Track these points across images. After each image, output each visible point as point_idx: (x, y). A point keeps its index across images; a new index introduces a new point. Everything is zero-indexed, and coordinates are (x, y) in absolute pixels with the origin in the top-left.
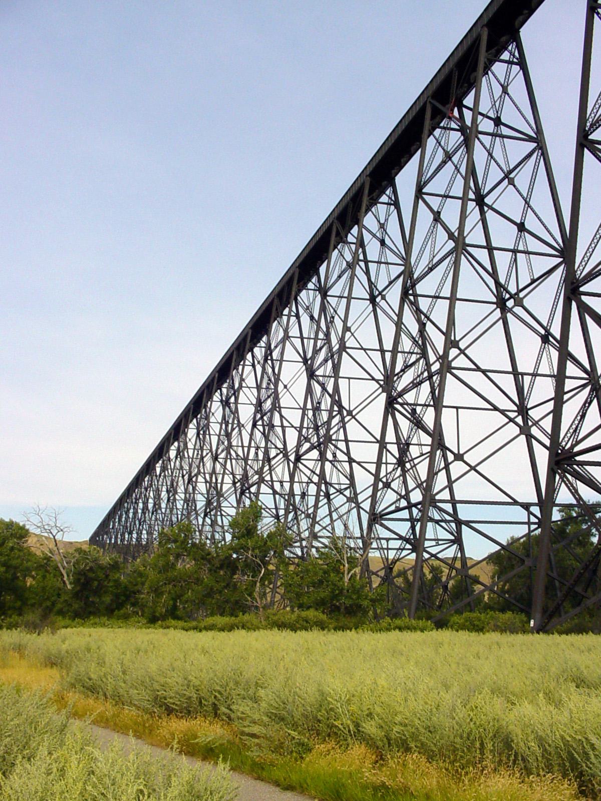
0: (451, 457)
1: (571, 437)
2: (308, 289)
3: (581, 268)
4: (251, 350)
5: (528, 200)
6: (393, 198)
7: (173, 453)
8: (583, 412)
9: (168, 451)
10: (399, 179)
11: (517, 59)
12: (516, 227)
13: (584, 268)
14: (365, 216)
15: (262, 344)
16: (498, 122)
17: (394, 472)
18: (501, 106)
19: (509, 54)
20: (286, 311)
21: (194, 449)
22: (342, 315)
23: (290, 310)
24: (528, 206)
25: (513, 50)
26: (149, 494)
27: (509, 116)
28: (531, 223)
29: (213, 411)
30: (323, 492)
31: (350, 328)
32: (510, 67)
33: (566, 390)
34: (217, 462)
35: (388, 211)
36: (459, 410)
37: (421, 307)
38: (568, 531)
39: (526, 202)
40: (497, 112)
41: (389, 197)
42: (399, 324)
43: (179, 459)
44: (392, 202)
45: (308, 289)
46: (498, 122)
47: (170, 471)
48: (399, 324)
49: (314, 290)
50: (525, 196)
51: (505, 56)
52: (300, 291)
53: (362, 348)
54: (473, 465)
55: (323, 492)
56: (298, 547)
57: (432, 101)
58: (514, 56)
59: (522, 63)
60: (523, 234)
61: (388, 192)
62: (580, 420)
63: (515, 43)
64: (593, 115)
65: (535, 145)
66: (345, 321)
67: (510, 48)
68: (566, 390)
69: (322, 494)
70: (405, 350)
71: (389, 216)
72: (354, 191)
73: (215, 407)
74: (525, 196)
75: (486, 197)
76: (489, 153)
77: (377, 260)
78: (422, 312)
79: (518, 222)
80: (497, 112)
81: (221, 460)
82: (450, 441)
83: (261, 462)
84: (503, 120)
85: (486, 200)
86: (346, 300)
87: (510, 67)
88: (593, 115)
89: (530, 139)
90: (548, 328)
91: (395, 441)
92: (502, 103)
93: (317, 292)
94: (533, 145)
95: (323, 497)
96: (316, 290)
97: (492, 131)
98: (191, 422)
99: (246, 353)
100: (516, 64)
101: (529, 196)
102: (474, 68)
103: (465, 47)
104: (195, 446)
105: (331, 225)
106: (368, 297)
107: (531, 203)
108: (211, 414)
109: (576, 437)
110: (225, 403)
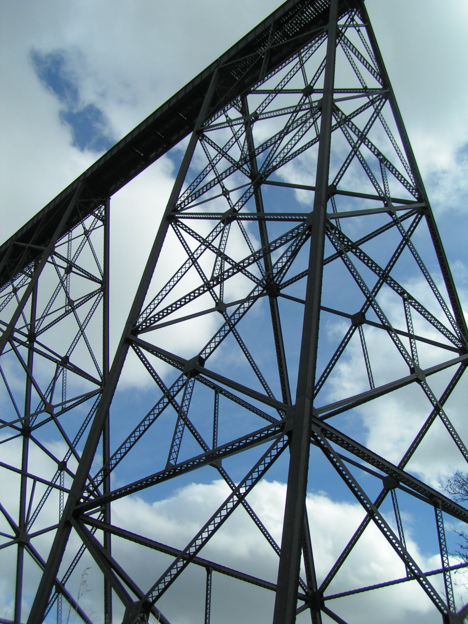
1: (276, 158)
3: (99, 298)
5: (83, 327)
8: (296, 246)
12: (57, 465)
13: (97, 298)
17: (42, 319)
33: (86, 549)
38: (461, 346)
39: (82, 332)
42: (277, 92)
48: (277, 92)
59: (105, 283)
60: (62, 473)
62: (290, 257)
64: (148, 311)
68: (86, 549)
75: (33, 430)
88: (148, 311)
90: (70, 452)
101: (85, 324)
109: (293, 118)
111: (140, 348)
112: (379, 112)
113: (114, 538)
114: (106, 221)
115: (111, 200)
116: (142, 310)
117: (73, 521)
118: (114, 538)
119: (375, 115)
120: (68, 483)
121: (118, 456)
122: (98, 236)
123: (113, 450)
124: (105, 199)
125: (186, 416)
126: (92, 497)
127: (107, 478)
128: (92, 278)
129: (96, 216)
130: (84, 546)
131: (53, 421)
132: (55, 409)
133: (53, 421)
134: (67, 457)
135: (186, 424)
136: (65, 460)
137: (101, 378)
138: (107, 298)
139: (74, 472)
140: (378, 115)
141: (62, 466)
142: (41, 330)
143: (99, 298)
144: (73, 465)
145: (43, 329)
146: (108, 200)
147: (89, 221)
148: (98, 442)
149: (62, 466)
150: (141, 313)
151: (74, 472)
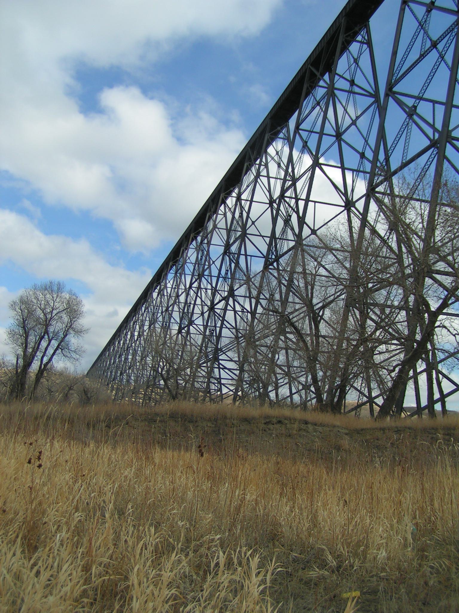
2: (233, 197)
4: (224, 202)
7: (155, 295)
9: (151, 294)
10: (375, 21)
11: (366, 40)
14: (339, 59)
15: (234, 194)
16: (352, 83)
19: (361, 37)
20: (258, 162)
21: (172, 288)
23: (261, 161)
25: (364, 34)
26: (136, 326)
27: (359, 80)
29: (189, 255)
32: (361, 45)
34: (191, 290)
35: (360, 49)
37: (210, 286)
41: (284, 134)
43: (160, 296)
45: (233, 197)
46: (352, 83)
47: (152, 307)
50: (365, 137)
51: (359, 38)
52: (226, 198)
53: (261, 236)
57: (312, 68)
58: (365, 39)
59: (369, 43)
61: (283, 131)
63: (365, 29)
65: (374, 99)
67: (362, 33)
70: (363, 174)
71: (361, 55)
72: (261, 129)
73: (192, 254)
74: (365, 137)
76: (345, 109)
77: (275, 177)
78: (296, 212)
79: (361, 152)
81: (194, 289)
84: (356, 82)
85: (343, 137)
86: (317, 135)
87: (361, 45)
89: (371, 95)
93: (286, 141)
94: (373, 99)
96: (285, 139)
97: (348, 89)
98: (191, 244)
99: (336, 58)
100: (365, 43)
101: (368, 137)
102: (333, 53)
103: (332, 32)
104: (172, 286)
105: (246, 152)
106: (334, 134)
107: (369, 142)
108: (187, 258)
110: (199, 249)
114: (369, 43)
115: (370, 23)
120: (368, 167)
121: (392, 148)
122: (365, 61)
123: (389, 146)
124: (365, 24)
125: (427, 32)
127: (388, 162)
129: (360, 42)
130: (383, 200)
134: (364, 148)
135: (428, 37)
136: (363, 152)
137: (374, 92)
138: (369, 35)
139: (371, 159)
141: (362, 155)
144: (369, 154)
146: (367, 23)
147: (354, 47)
148: (380, 145)
149: (362, 155)
151: (371, 159)
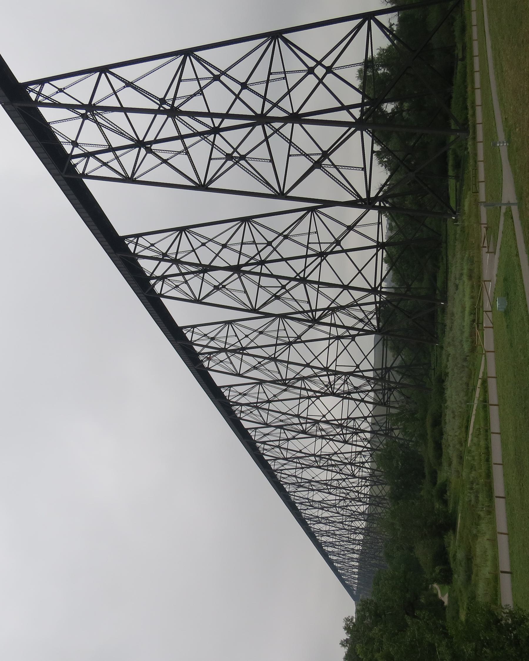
0: (358, 370)
3: (179, 119)
6: (227, 388)
18: (66, 138)
22: (294, 453)
24: (212, 240)
28: (223, 240)
30: (347, 396)
31: (300, 450)
32: (150, 273)
33: (116, 152)
36: (337, 365)
40: (69, 142)
44: (229, 389)
49: (256, 432)
54: (367, 357)
55: (347, 396)
56: (383, 288)
66: (297, 452)
68: (116, 152)
69: (348, 396)
80: (69, 142)
82: (352, 369)
83: (339, 495)
87: (150, 273)
91: (328, 340)
92: (60, 134)
95: (350, 396)
111: (199, 183)
112: (47, 97)
113: (381, 399)
116: (52, 102)
117: (257, 311)
118: (381, 399)
119: (50, 99)
126: (393, 411)
128: (183, 63)
131: (298, 273)
132: (244, 161)
133: (298, 273)
140: (34, 90)
142: (125, 174)
143: (179, 119)
145: (124, 172)
150: (52, 102)
